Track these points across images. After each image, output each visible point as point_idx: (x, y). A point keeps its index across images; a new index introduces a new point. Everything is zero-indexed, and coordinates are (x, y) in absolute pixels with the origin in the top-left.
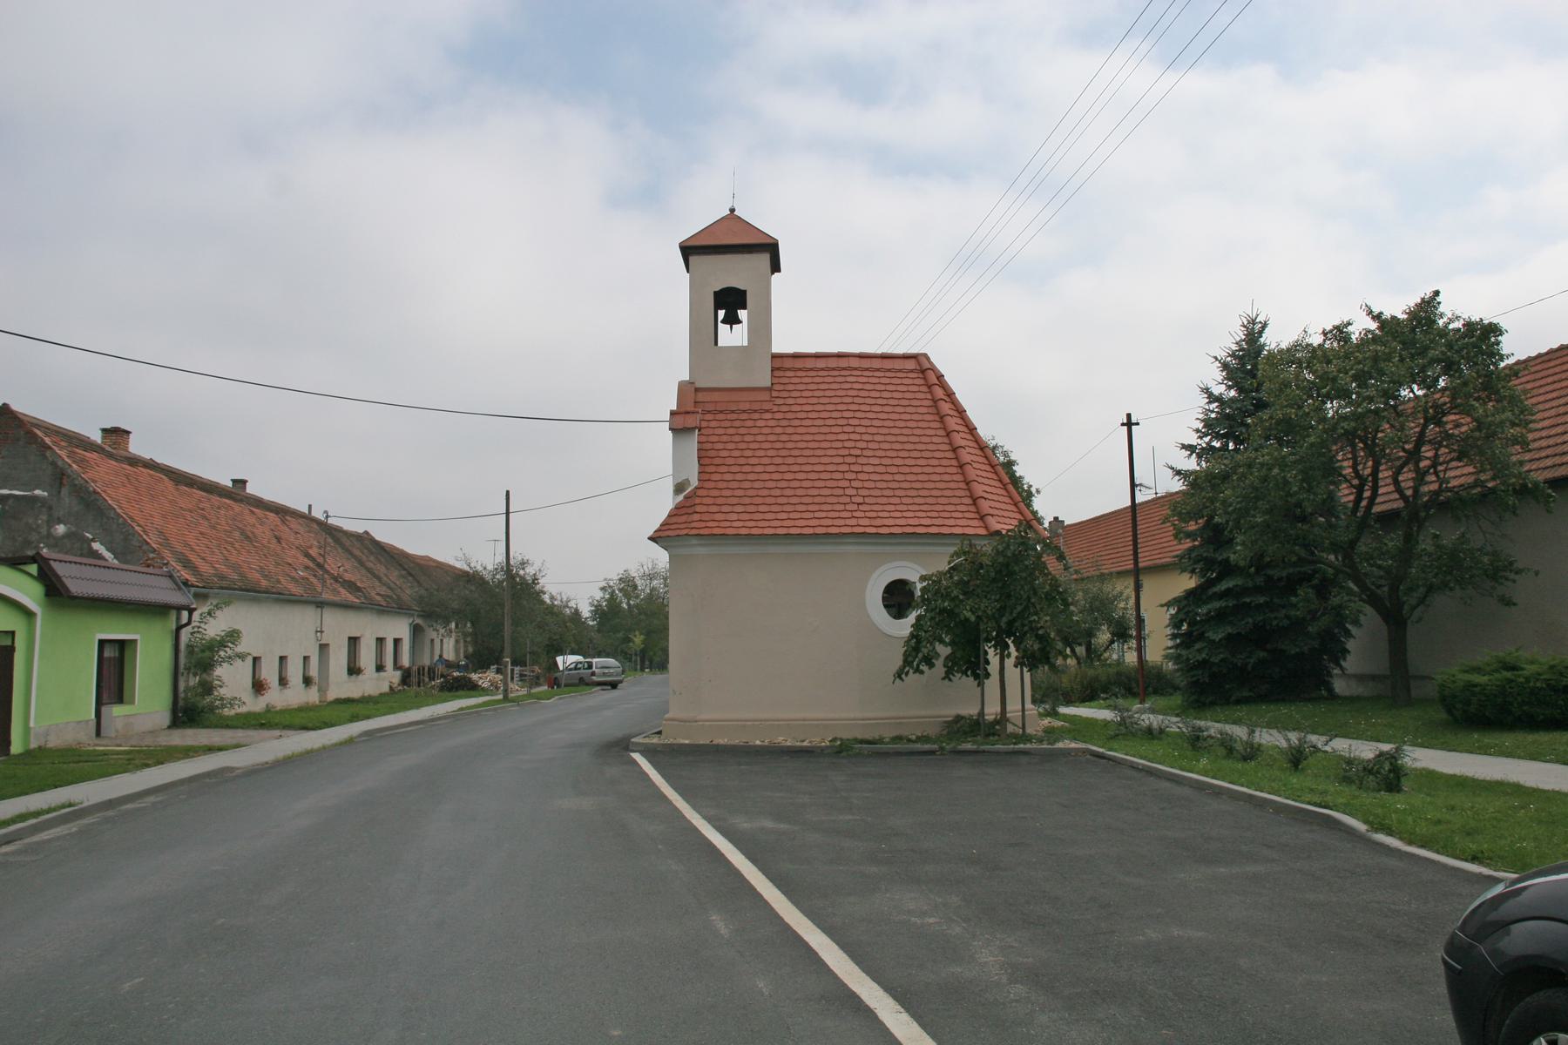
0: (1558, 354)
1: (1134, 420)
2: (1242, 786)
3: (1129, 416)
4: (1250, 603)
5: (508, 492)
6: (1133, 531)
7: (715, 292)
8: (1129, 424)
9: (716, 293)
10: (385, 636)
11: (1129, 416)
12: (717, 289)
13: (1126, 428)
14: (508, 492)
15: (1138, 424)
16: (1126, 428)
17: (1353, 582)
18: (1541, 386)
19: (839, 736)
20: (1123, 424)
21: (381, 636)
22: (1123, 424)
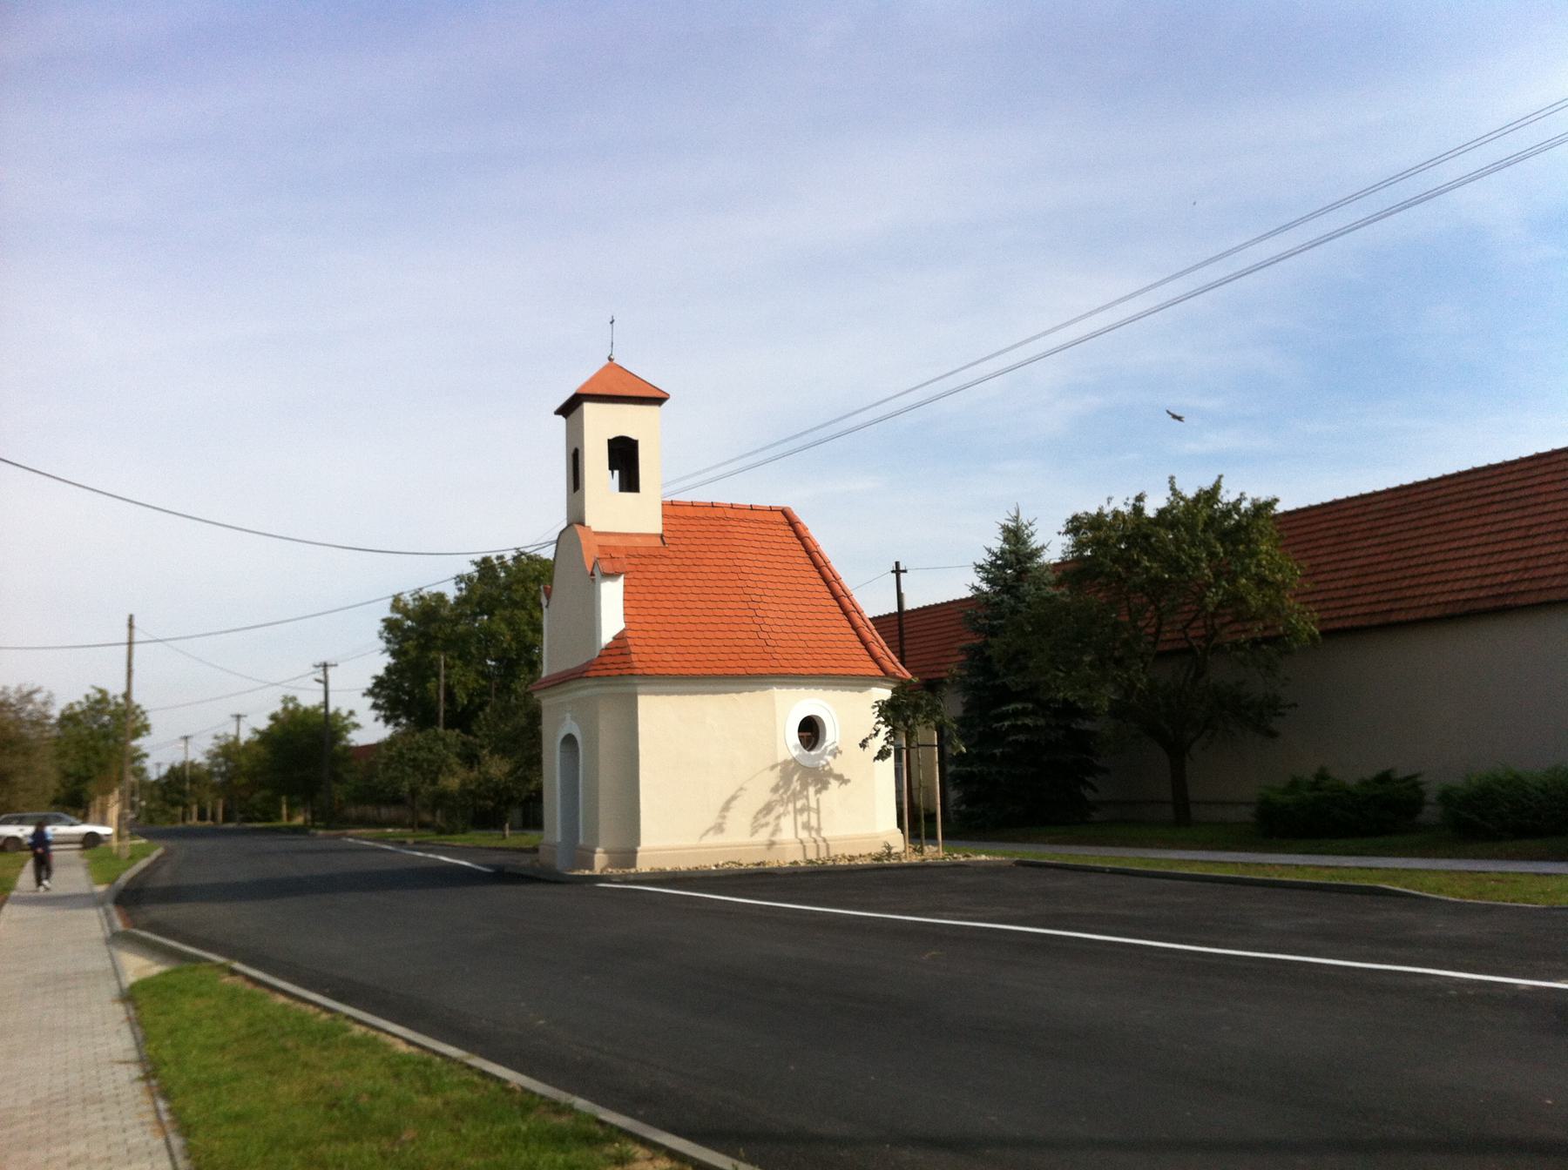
0: (922, 612)
1: (902, 568)
2: (1435, 894)
3: (897, 564)
4: (1001, 727)
5: (131, 619)
6: (904, 656)
7: (609, 441)
8: (898, 571)
9: (611, 442)
10: (1141, 491)
11: (897, 564)
12: (611, 438)
13: (894, 575)
14: (131, 619)
15: (905, 571)
16: (894, 575)
17: (143, 844)
18: (1343, 560)
19: (754, 813)
20: (893, 572)
21: (1138, 494)
22: (893, 572)
